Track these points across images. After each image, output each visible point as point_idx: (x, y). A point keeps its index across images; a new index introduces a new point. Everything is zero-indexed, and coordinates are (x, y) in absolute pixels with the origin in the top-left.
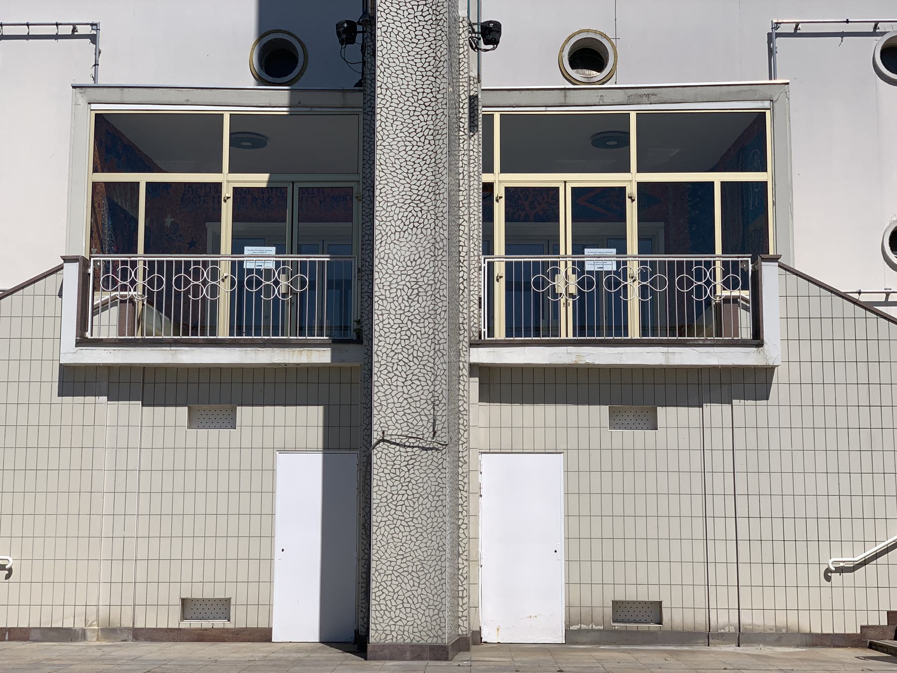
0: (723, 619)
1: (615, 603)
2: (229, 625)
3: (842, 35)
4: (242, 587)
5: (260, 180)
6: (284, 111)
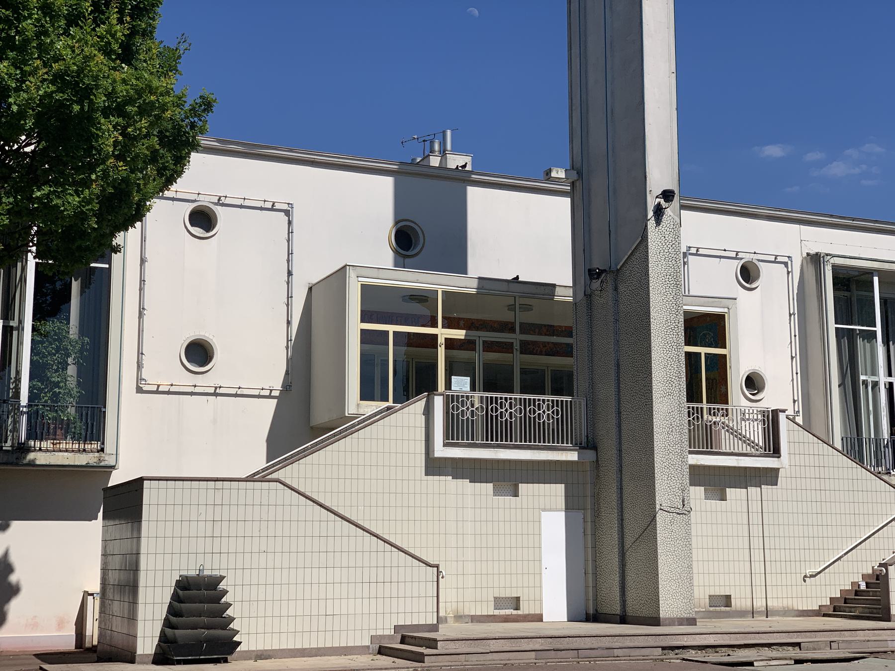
0: (759, 604)
1: (710, 596)
2: (519, 612)
3: (720, 257)
4: (526, 590)
5: (459, 334)
6: (474, 291)
